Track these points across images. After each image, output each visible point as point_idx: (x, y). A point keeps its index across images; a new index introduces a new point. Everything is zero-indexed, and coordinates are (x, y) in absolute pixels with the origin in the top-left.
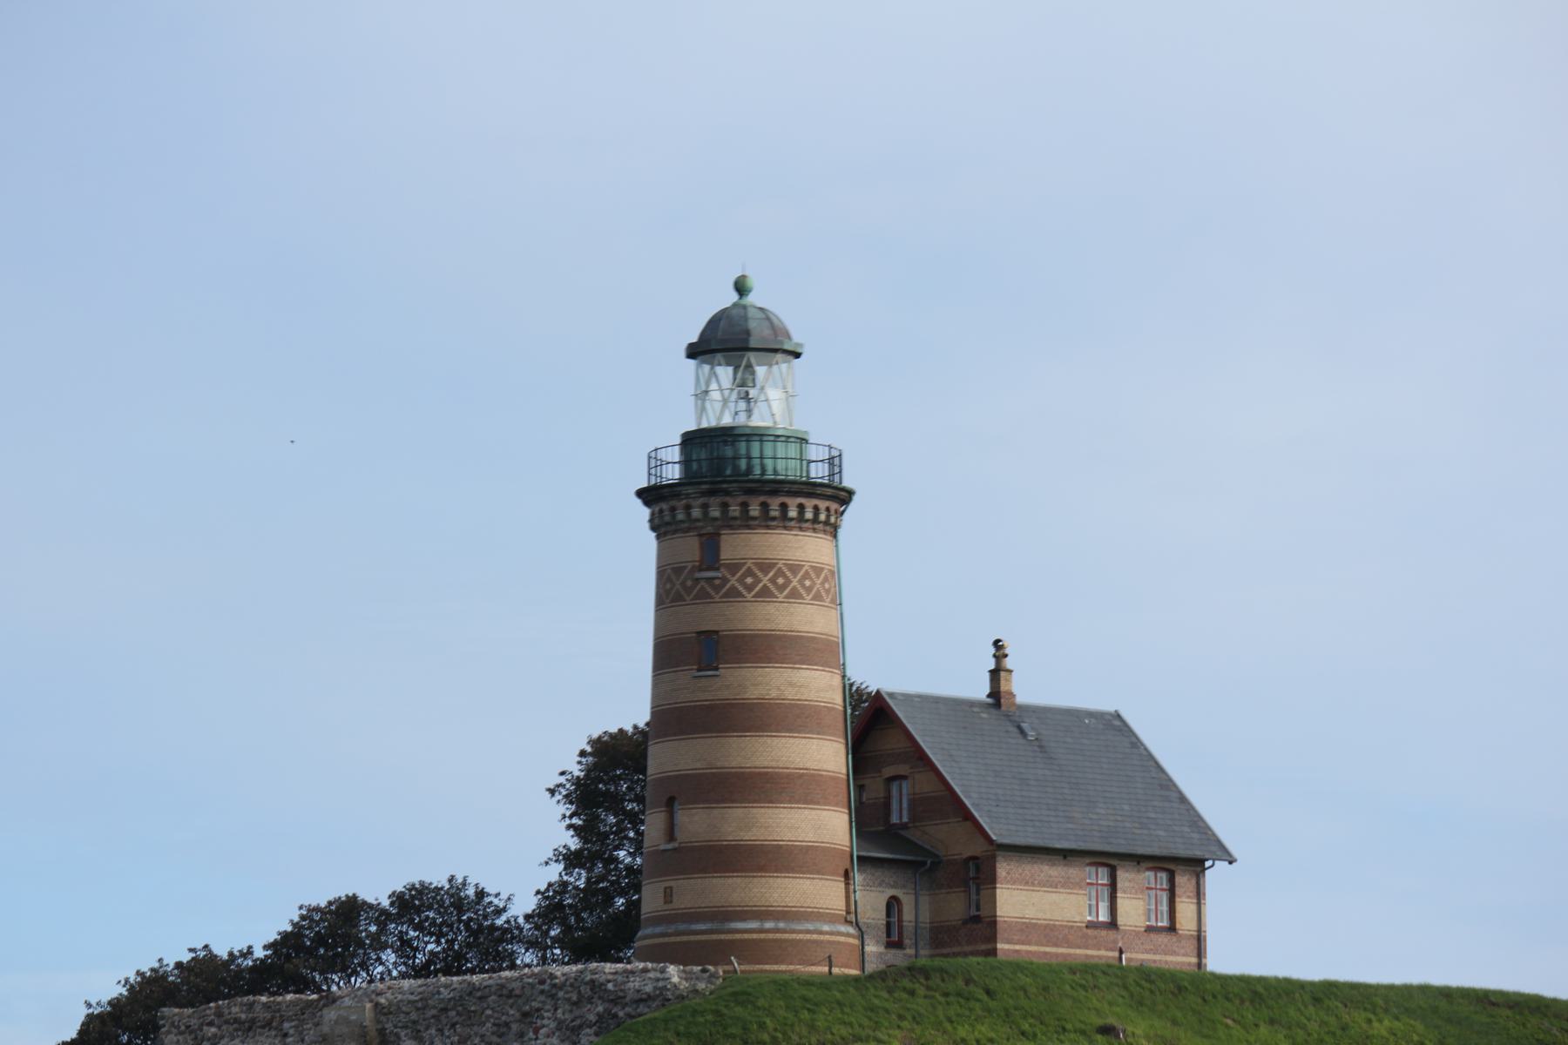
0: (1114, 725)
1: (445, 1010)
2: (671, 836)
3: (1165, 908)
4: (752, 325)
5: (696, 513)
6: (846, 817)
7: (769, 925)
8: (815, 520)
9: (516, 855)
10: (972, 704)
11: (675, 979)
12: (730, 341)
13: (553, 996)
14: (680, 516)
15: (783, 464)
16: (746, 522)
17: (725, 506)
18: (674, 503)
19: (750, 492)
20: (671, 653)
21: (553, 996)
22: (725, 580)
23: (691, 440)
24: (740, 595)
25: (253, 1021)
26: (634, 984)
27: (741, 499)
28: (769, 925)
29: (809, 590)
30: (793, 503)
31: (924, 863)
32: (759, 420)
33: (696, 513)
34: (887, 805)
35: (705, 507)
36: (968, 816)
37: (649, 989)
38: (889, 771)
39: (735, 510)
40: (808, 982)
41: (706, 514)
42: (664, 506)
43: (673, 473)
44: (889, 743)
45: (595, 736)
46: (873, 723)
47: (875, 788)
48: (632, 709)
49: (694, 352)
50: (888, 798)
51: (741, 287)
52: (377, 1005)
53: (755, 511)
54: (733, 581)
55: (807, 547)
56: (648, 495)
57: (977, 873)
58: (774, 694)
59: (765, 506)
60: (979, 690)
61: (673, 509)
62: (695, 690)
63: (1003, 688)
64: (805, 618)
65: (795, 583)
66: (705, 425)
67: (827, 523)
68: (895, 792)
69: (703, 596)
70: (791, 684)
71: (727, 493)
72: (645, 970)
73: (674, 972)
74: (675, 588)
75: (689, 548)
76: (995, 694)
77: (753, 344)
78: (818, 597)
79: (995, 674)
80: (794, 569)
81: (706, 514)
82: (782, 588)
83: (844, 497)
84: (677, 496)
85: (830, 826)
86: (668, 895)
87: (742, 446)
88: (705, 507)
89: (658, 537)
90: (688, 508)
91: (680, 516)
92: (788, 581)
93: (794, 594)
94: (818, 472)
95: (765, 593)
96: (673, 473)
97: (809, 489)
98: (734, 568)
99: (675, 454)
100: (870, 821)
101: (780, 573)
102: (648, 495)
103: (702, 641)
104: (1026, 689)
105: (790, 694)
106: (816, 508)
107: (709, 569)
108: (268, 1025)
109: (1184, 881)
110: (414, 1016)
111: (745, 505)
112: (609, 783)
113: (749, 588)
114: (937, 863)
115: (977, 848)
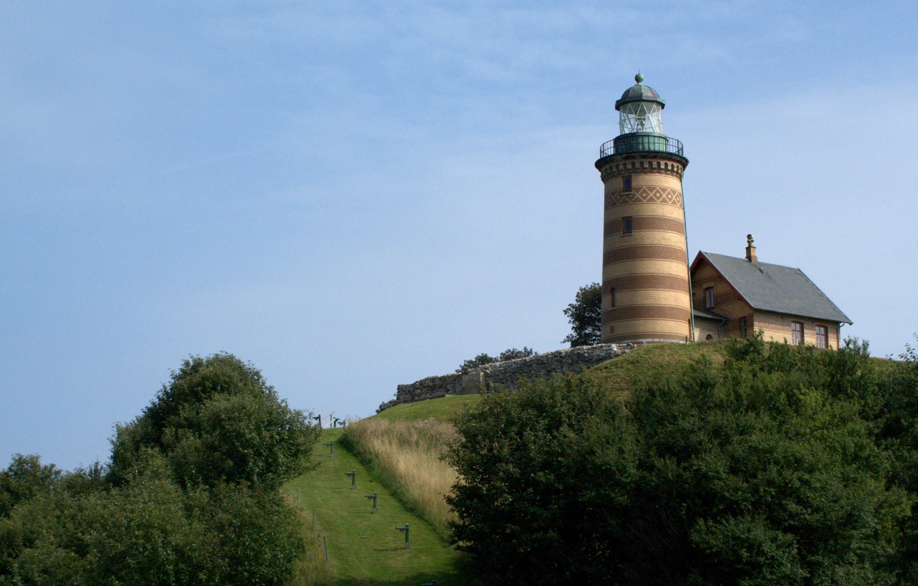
0: (798, 273)
1: (514, 373)
2: (613, 305)
3: (824, 343)
4: (643, 91)
5: (621, 167)
6: (688, 297)
7: (656, 340)
8: (672, 171)
9: (551, 334)
10: (739, 260)
11: (615, 349)
12: (632, 102)
13: (561, 362)
14: (615, 169)
15: (660, 147)
16: (644, 171)
17: (634, 164)
18: (652, 160)
19: (644, 157)
20: (611, 257)
21: (561, 362)
22: (634, 195)
23: (618, 141)
24: (640, 200)
25: (435, 386)
26: (597, 352)
27: (640, 160)
28: (656, 340)
29: (670, 199)
30: (663, 163)
31: (721, 321)
32: (647, 129)
33: (621, 167)
34: (705, 300)
35: (625, 165)
36: (741, 298)
37: (603, 354)
38: (705, 286)
39: (637, 165)
40: (675, 345)
41: (625, 167)
42: (607, 167)
43: (610, 151)
44: (705, 273)
45: (583, 287)
46: (701, 265)
47: (700, 294)
48: (594, 276)
49: (619, 105)
50: (705, 297)
51: (638, 79)
52: (486, 373)
53: (646, 166)
54: (638, 195)
55: (670, 182)
56: (599, 164)
57: (745, 324)
58: (656, 242)
59: (650, 163)
60: (743, 255)
61: (611, 168)
62: (621, 269)
63: (752, 254)
64: (671, 212)
65: (664, 196)
66: (627, 131)
67: (677, 173)
68: (708, 295)
69: (625, 202)
70: (664, 238)
71: (634, 158)
72: (602, 347)
73: (614, 347)
74: (611, 201)
75: (619, 183)
76: (749, 257)
77: (644, 98)
78: (674, 203)
79: (748, 249)
80: (664, 190)
81: (625, 167)
82: (658, 198)
83: (684, 162)
84: (612, 161)
85: (682, 300)
86: (612, 329)
87: (640, 140)
88: (625, 165)
89: (604, 179)
90: (617, 166)
91: (615, 169)
92: (661, 195)
93: (664, 201)
94: (672, 150)
95: (651, 200)
96: (610, 151)
97: (669, 156)
98: (637, 190)
99: (612, 144)
100: (697, 304)
101: (658, 191)
102: (599, 164)
103: (624, 230)
104: (762, 255)
105: (663, 242)
106: (673, 166)
107: (628, 191)
108: (441, 387)
109: (831, 329)
110: (501, 377)
111: (642, 163)
112: (589, 311)
113: (645, 198)
114: (727, 321)
115: (746, 312)
